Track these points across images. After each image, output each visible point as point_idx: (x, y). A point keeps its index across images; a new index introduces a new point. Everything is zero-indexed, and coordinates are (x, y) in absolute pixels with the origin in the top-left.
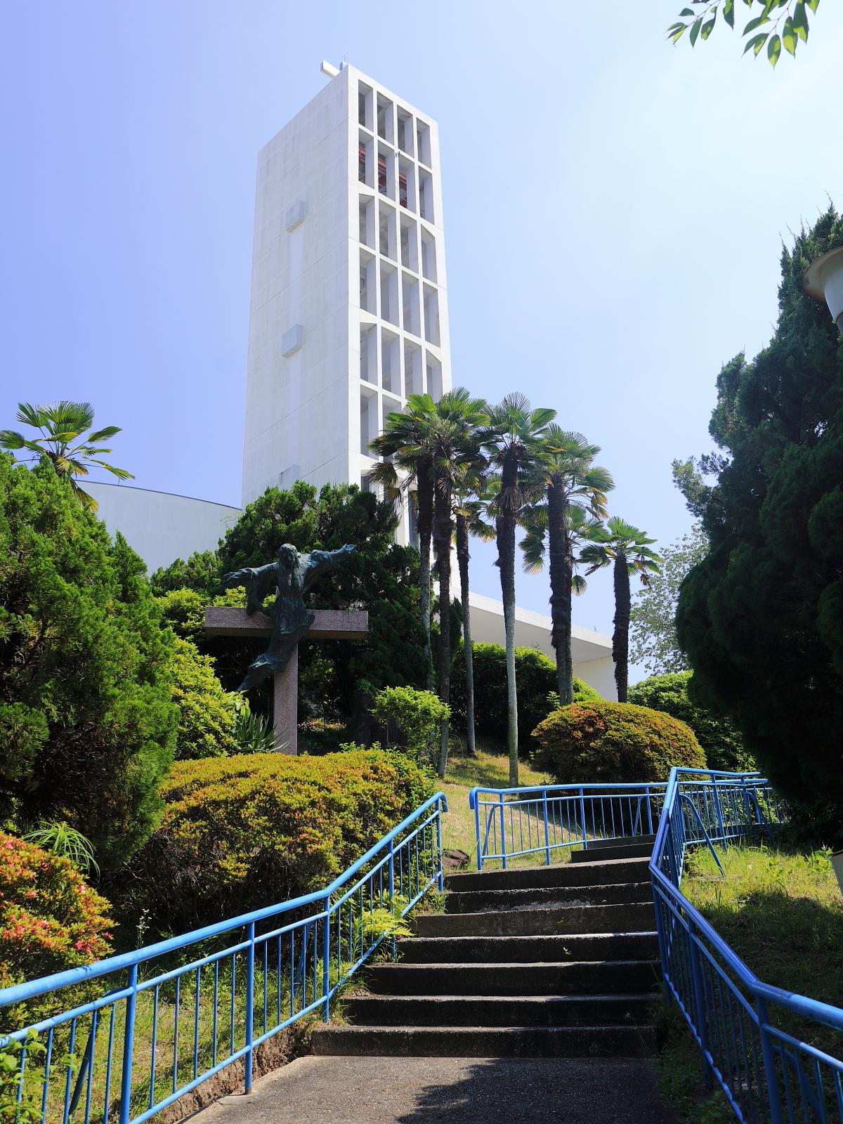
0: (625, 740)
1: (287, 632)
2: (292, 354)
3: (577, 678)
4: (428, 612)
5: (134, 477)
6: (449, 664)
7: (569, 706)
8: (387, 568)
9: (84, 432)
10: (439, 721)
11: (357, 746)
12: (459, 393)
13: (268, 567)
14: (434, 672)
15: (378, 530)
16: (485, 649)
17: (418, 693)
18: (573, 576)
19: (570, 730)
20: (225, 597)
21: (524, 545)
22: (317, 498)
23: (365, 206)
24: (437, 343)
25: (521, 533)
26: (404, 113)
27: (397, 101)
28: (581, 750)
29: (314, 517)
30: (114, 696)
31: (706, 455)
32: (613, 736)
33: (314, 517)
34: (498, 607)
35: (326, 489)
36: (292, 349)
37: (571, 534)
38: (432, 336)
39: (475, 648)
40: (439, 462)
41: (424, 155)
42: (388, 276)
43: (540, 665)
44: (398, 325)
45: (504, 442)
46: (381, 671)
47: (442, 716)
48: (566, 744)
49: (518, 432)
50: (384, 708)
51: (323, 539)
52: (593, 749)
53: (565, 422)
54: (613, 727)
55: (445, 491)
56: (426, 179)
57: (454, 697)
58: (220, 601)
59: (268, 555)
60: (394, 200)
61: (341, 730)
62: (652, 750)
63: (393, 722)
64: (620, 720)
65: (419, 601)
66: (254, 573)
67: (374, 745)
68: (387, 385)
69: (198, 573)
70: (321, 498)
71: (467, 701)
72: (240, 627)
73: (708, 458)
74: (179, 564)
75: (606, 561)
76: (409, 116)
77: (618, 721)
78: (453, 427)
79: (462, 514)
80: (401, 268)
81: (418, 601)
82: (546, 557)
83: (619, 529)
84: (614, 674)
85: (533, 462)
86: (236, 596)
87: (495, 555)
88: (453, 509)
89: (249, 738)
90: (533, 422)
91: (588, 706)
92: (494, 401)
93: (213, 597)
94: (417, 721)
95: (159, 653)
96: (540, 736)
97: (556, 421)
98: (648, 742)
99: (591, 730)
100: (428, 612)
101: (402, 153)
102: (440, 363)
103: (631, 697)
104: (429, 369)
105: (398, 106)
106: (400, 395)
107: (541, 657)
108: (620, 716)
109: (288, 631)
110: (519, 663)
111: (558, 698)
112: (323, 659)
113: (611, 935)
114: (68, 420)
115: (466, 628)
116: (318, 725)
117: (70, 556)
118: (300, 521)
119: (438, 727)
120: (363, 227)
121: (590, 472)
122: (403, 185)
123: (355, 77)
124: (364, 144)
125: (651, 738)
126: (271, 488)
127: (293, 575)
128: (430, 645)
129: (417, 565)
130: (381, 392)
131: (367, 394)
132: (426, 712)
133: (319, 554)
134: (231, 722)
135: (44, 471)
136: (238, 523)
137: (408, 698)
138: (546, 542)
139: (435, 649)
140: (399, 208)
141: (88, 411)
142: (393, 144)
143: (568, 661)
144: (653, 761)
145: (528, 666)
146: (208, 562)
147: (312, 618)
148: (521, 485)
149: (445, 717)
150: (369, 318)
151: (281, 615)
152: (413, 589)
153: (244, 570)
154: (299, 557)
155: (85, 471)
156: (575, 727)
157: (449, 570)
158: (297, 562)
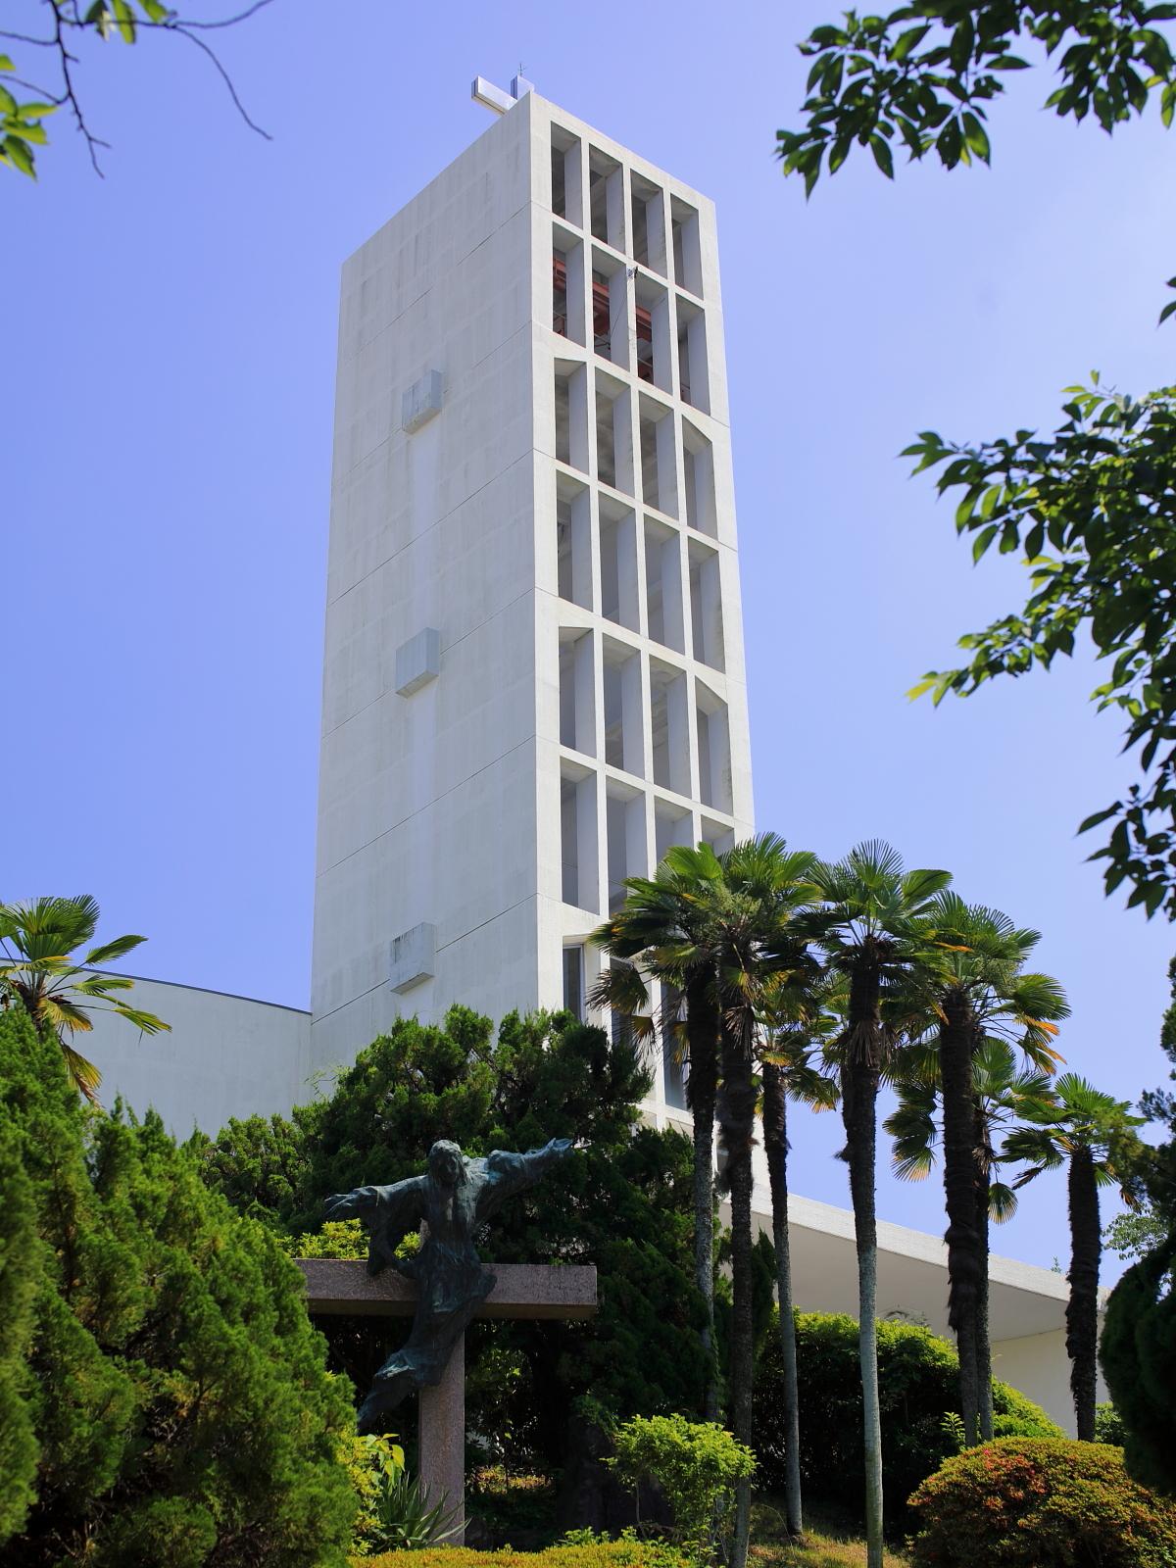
0: (1083, 1514)
1: (445, 1310)
2: (417, 689)
3: (1003, 1382)
4: (710, 1262)
5: (170, 1028)
6: (751, 1365)
7: (980, 1447)
8: (627, 1176)
9: (80, 947)
10: (734, 1481)
11: (595, 1535)
12: (766, 842)
13: (409, 1185)
14: (722, 1380)
15: (609, 1100)
16: (821, 1327)
17: (695, 1428)
18: (991, 1185)
19: (981, 1495)
20: (321, 1237)
21: (896, 1124)
22: (493, 1041)
23: (567, 381)
24: (719, 665)
25: (888, 1101)
26: (645, 186)
27: (631, 161)
28: (1002, 1532)
29: (490, 1079)
30: (289, 1483)
31: (1148, 1092)
32: (1061, 1507)
33: (490, 1079)
34: (843, 1223)
35: (511, 1022)
36: (417, 679)
37: (988, 1103)
38: (709, 650)
39: (802, 1324)
40: (728, 978)
41: (687, 271)
42: (615, 524)
43: (928, 1358)
44: (637, 630)
45: (853, 934)
46: (620, 1381)
47: (738, 1470)
48: (973, 1522)
49: (879, 913)
50: (630, 1455)
51: (506, 1119)
52: (1022, 1530)
53: (971, 891)
54: (1062, 1488)
55: (738, 1033)
56: (691, 321)
57: (758, 1430)
58: (311, 1245)
59: (401, 1153)
60: (626, 367)
61: (540, 1487)
62: (1135, 1534)
63: (645, 1481)
64: (1075, 1475)
65: (693, 1241)
66: (381, 1197)
67: (625, 1533)
68: (615, 756)
69: (240, 1162)
70: (502, 1039)
71: (786, 1428)
72: (355, 1297)
73: (1152, 1095)
74: (198, 1144)
75: (1053, 1157)
76: (656, 191)
77: (1072, 1477)
78: (755, 906)
79: (772, 1063)
80: (642, 509)
81: (690, 1241)
82: (937, 1146)
83: (1076, 1098)
84: (1068, 1380)
85: (908, 966)
86: (343, 1237)
87: (841, 1140)
88: (755, 1051)
89: (398, 1517)
90: (907, 895)
91: (1015, 1447)
92: (834, 854)
93: (298, 1236)
94: (692, 1482)
95: (338, 1414)
96: (924, 1505)
97: (953, 887)
98: (1128, 1518)
99: (1021, 1494)
100: (710, 1262)
101: (642, 269)
102: (726, 705)
103: (1104, 1425)
104: (702, 718)
105: (633, 172)
106: (642, 775)
107: (932, 1343)
108: (1075, 1468)
109: (449, 1306)
110: (886, 1356)
111: (963, 1426)
112: (503, 1349)
114: (54, 929)
115: (783, 1289)
116: (492, 1480)
117: (220, 1281)
118: (463, 1088)
119: (732, 1491)
120: (563, 422)
121: (1021, 984)
122: (644, 331)
123: (543, 116)
124: (565, 251)
125: (1133, 1510)
126: (405, 1019)
127: (456, 1199)
128: (714, 1327)
129: (687, 1169)
130: (603, 770)
131: (575, 776)
132: (710, 1464)
133: (504, 1160)
134: (372, 1492)
135: (156, 1138)
136: (338, 1086)
137: (677, 1438)
138: (937, 1116)
139: (723, 1334)
140: (638, 385)
141: (88, 909)
142: (624, 253)
143: (982, 1354)
144: (1137, 1554)
145: (904, 1359)
146: (259, 1139)
147: (491, 1281)
148: (889, 1009)
149: (745, 1472)
150: (576, 617)
151: (433, 1276)
152: (680, 1218)
153: (363, 1190)
154: (466, 1164)
155: (85, 1022)
156: (990, 1490)
157: (749, 1183)
158: (462, 1175)
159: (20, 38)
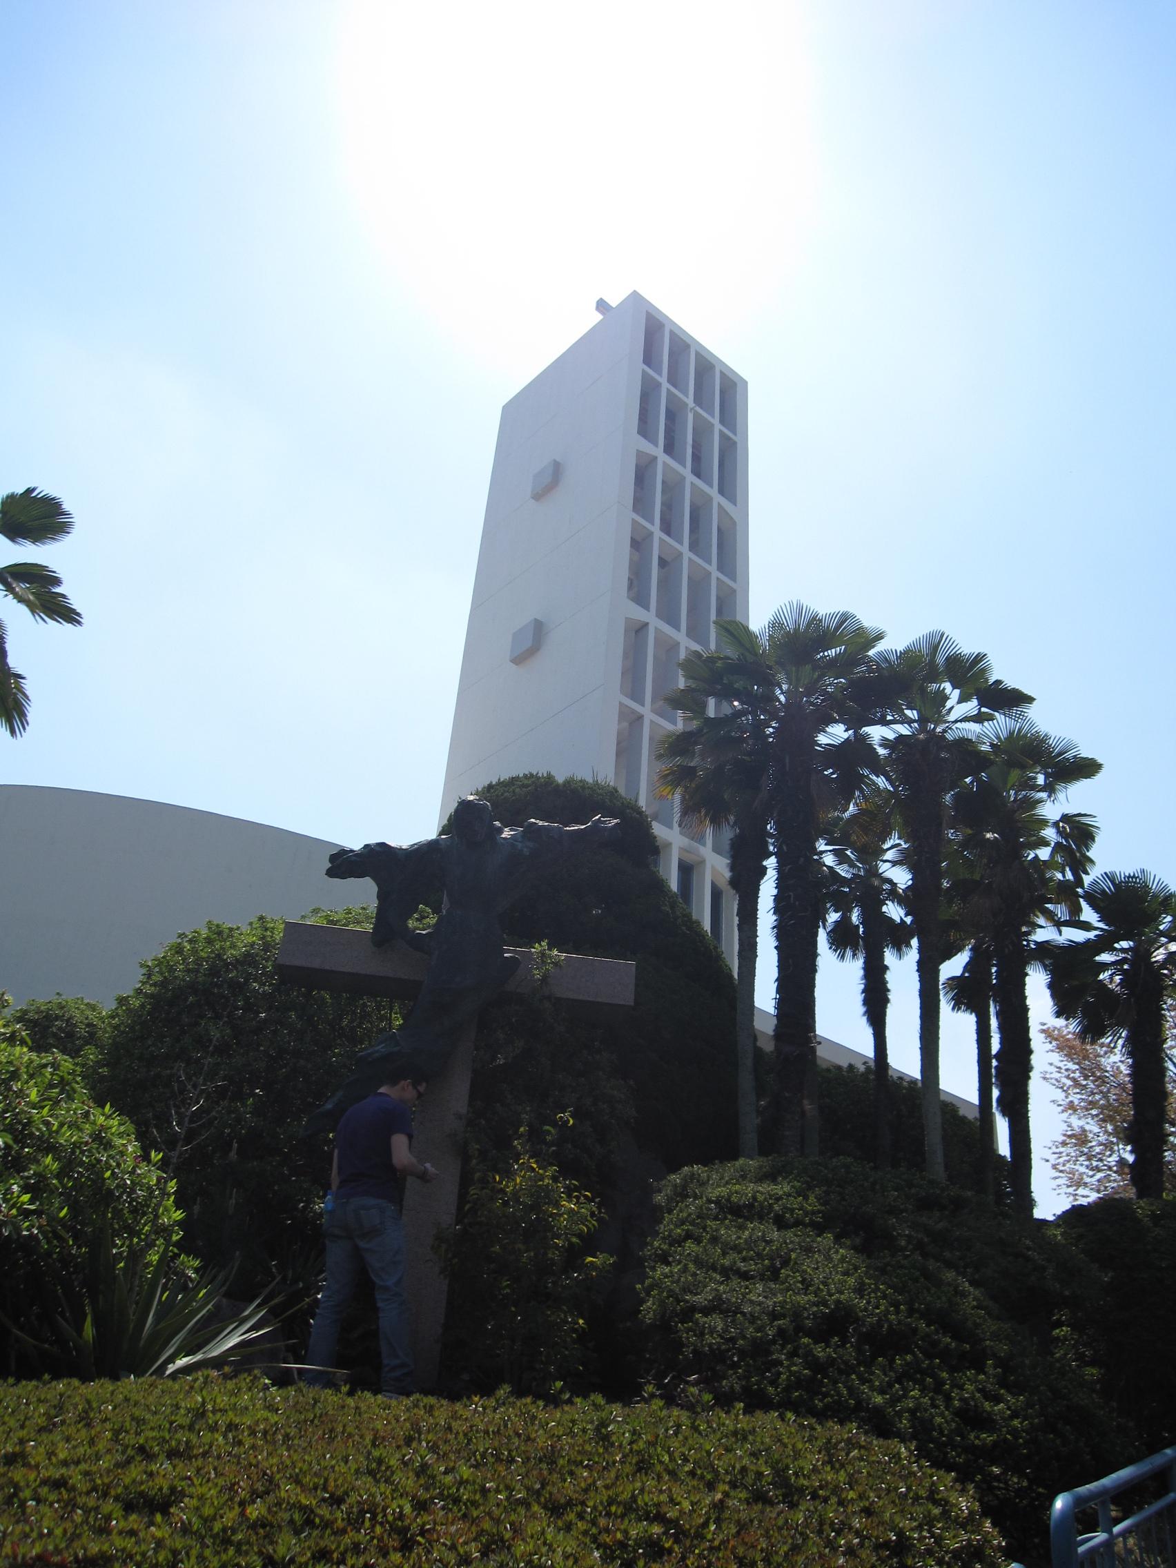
101: (698, 409)
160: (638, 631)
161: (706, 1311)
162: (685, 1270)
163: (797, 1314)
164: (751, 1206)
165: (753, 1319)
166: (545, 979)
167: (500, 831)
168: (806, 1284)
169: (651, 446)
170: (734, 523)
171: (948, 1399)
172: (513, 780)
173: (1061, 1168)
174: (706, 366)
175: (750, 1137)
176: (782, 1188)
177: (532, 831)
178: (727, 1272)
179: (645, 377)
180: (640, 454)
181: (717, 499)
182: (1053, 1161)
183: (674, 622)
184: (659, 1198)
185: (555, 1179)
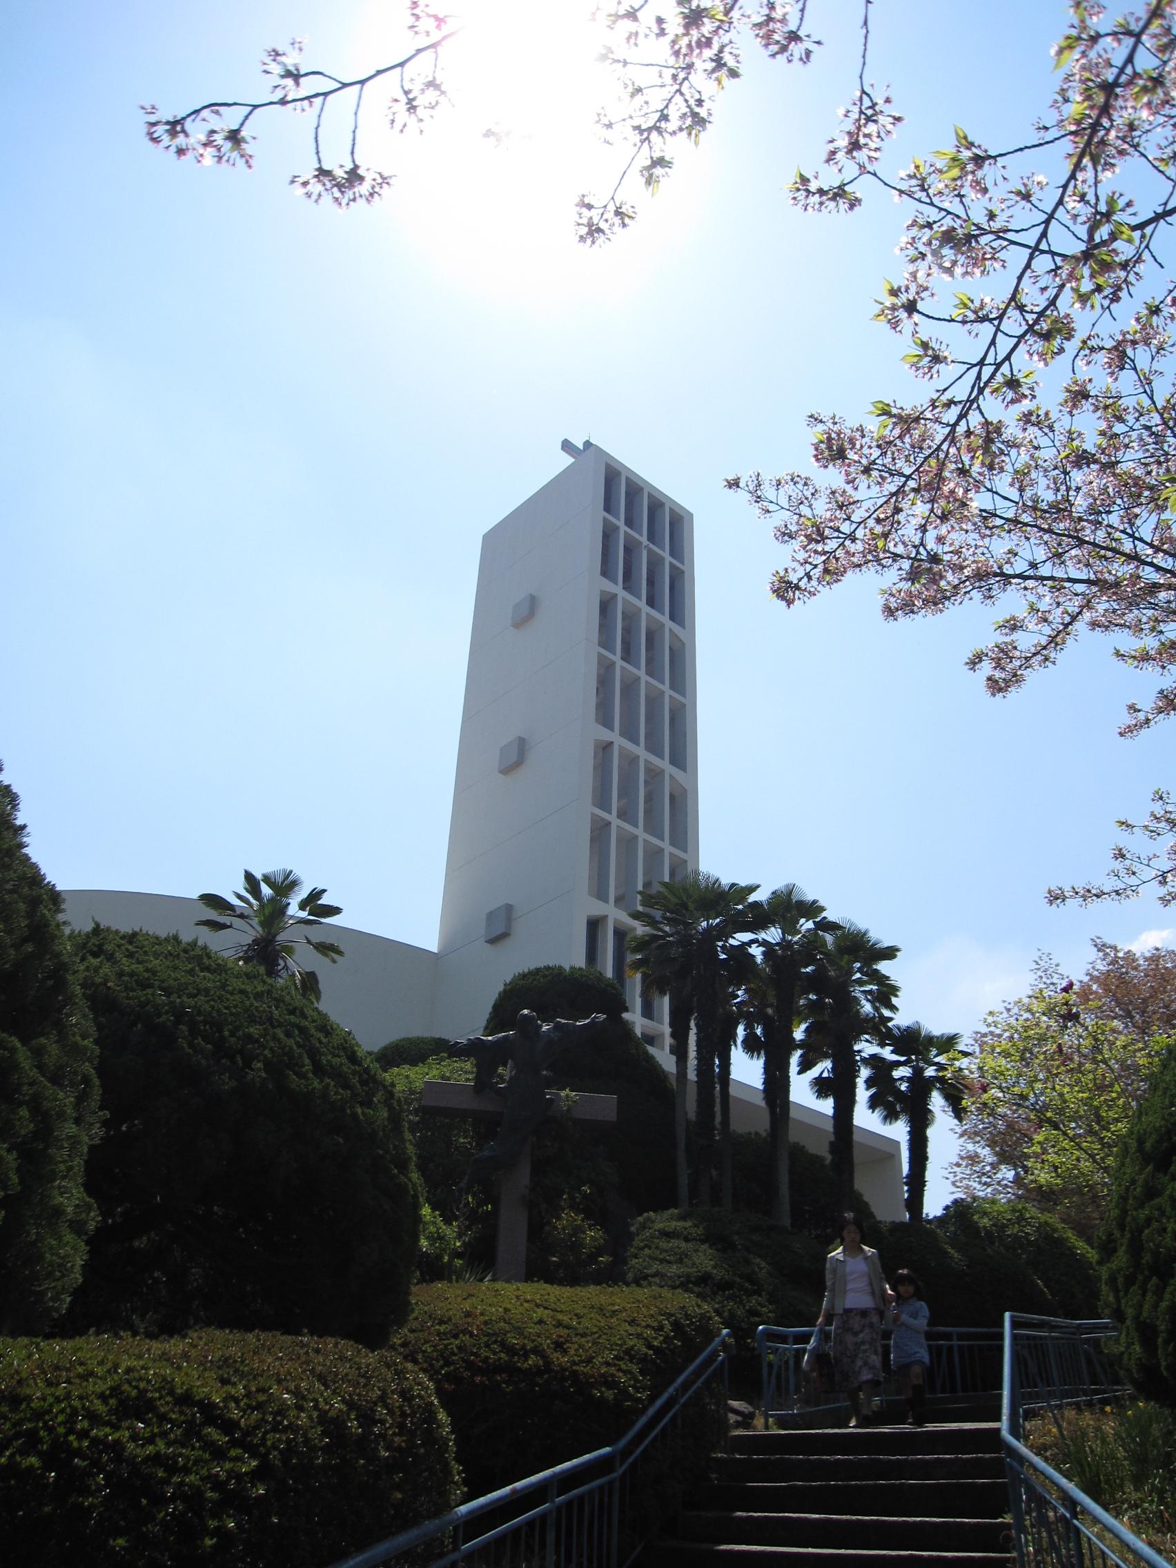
42: (630, 688)
101: (651, 546)
104: (672, 797)
113: (608, 1449)
122: (651, 582)
140: (646, 609)
159: (353, 149)
160: (605, 748)
161: (653, 1276)
162: (644, 1260)
163: (688, 1276)
164: (674, 1232)
165: (671, 1278)
166: (568, 1110)
167: (541, 1026)
168: (694, 1264)
169: (612, 584)
170: (683, 644)
171: (744, 1306)
172: (538, 970)
173: (959, 1184)
174: (657, 504)
175: (684, 1191)
176: (688, 1224)
177: (558, 1026)
178: (662, 1261)
179: (606, 523)
180: (603, 593)
181: (669, 624)
182: (952, 1179)
183: (634, 740)
184: (633, 1229)
185: (583, 1220)
